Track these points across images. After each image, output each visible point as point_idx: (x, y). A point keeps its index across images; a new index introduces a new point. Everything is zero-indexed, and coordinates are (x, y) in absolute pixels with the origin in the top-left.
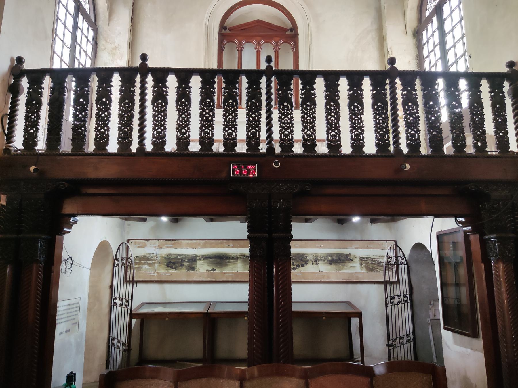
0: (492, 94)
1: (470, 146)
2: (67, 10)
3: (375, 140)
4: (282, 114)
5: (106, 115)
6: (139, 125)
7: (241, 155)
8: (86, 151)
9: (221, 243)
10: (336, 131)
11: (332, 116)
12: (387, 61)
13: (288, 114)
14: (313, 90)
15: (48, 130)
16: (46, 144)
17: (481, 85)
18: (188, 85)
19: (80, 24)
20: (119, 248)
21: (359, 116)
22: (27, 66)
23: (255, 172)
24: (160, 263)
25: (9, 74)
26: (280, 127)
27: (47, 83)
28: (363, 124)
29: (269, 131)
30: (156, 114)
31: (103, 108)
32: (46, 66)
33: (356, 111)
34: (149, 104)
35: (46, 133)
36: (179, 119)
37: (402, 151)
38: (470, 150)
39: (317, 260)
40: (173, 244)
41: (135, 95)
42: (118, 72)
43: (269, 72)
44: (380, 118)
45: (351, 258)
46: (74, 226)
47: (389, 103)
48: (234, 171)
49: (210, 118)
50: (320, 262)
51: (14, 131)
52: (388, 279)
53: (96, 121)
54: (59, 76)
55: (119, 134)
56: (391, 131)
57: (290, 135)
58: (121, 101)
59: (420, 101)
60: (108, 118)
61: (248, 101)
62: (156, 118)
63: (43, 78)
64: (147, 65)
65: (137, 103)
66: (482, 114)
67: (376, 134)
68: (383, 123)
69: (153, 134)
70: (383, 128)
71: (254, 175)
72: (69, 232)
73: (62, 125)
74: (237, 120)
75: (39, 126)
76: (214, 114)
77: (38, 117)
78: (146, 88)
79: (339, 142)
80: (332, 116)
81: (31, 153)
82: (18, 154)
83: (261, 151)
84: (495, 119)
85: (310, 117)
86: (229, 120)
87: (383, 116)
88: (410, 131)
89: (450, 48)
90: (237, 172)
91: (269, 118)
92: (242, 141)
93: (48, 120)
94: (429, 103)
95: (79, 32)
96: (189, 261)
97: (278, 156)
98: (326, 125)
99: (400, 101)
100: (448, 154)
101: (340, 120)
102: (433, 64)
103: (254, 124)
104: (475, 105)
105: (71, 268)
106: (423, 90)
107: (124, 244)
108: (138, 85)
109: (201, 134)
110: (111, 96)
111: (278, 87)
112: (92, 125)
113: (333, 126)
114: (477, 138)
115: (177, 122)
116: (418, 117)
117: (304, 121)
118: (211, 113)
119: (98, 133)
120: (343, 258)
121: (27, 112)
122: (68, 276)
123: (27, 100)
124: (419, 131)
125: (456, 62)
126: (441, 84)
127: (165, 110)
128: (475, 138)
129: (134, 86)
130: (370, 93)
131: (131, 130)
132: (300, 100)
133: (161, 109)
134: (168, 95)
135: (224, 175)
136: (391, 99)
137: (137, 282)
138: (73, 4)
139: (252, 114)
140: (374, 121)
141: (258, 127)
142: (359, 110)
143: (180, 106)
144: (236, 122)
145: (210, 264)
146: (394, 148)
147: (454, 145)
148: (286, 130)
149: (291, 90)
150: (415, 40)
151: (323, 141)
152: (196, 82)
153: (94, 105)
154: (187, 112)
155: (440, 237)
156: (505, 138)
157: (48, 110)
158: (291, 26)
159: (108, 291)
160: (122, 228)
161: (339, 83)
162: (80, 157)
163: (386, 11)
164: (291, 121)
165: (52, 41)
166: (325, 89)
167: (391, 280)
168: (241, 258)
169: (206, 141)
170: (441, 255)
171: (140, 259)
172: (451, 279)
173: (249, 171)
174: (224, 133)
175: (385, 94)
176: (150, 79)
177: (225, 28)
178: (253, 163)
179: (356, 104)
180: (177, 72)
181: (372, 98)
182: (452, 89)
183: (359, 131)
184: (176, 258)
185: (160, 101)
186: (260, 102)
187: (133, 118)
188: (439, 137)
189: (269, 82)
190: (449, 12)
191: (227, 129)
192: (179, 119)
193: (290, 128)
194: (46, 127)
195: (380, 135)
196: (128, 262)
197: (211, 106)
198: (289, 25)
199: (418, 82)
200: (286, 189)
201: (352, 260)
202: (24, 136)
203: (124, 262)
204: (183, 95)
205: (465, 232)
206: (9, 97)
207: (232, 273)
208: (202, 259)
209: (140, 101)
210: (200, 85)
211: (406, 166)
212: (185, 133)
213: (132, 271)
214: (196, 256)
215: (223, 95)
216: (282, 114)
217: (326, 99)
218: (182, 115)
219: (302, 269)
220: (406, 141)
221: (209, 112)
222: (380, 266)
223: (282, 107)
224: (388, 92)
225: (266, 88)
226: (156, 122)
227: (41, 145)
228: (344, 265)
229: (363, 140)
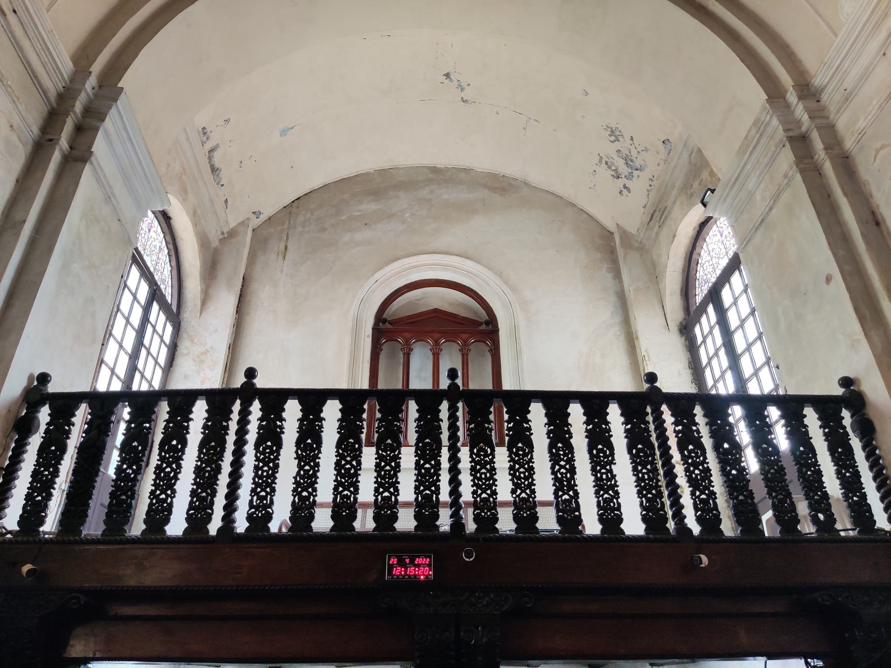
4: (477, 463)
7: (405, 536)
10: (571, 493)
11: (562, 467)
12: (643, 378)
13: (486, 463)
15: (69, 496)
17: (805, 416)
18: (319, 416)
21: (608, 467)
23: (430, 570)
25: (20, 402)
26: (472, 486)
27: (82, 415)
28: (616, 481)
31: (170, 457)
32: (85, 388)
33: (602, 458)
34: (250, 449)
37: (690, 531)
41: (227, 434)
43: (453, 394)
44: (644, 471)
47: (656, 445)
48: (391, 567)
53: (155, 480)
54: (103, 405)
55: (191, 502)
56: (666, 493)
59: (707, 442)
60: (176, 474)
62: (260, 472)
64: (254, 385)
65: (230, 447)
66: (816, 464)
67: (641, 498)
68: (650, 479)
69: (251, 502)
71: (427, 576)
73: (93, 487)
74: (399, 474)
77: (56, 473)
79: (577, 513)
80: (562, 467)
83: (442, 529)
84: (838, 472)
85: (524, 468)
89: (737, 329)
92: (407, 505)
97: (473, 538)
98: (552, 482)
99: (673, 442)
108: (235, 417)
111: (467, 418)
112: (147, 483)
115: (295, 478)
116: (708, 470)
118: (354, 463)
119: (154, 501)
123: (42, 443)
128: (810, 506)
130: (622, 428)
131: (214, 493)
133: (266, 481)
134: (283, 433)
136: (657, 438)
138: (147, 288)
140: (634, 475)
142: (606, 456)
143: (302, 452)
144: (397, 478)
146: (676, 524)
148: (484, 491)
149: (489, 422)
150: (683, 338)
152: (332, 411)
154: (314, 461)
161: (569, 411)
162: (116, 547)
163: (632, 296)
164: (492, 475)
166: (545, 420)
175: (647, 430)
176: (256, 408)
177: (384, 321)
179: (600, 447)
180: (302, 395)
181: (626, 437)
183: (610, 492)
185: (269, 443)
187: (220, 473)
189: (453, 410)
191: (381, 490)
193: (491, 488)
195: (648, 500)
198: (484, 316)
199: (698, 410)
204: (310, 433)
210: (339, 415)
211: (700, 558)
215: (377, 432)
216: (477, 463)
217: (549, 437)
218: (304, 466)
221: (352, 460)
223: (475, 451)
224: (652, 427)
225: (449, 419)
227: (50, 525)
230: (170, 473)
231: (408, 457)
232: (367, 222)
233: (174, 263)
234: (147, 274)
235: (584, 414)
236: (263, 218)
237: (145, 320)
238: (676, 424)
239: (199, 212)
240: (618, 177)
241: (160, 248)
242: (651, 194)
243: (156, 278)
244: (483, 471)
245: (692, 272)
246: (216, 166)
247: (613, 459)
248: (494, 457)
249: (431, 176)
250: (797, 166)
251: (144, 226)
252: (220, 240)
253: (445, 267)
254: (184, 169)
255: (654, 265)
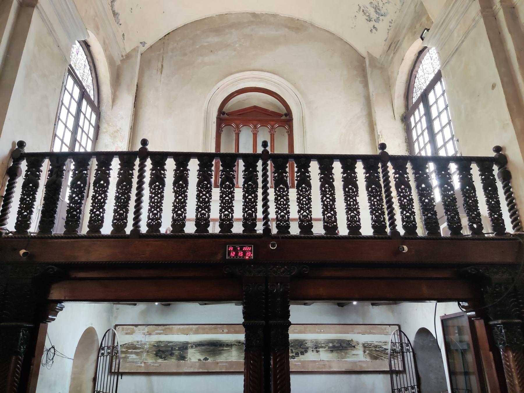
0: (483, 177)
1: (465, 226)
2: (72, 97)
3: (371, 222)
4: (278, 196)
5: (102, 198)
6: (135, 207)
7: (237, 236)
8: (79, 233)
9: (215, 328)
10: (332, 212)
11: (327, 198)
12: (378, 146)
13: (284, 196)
14: (308, 173)
15: (43, 212)
16: (39, 226)
17: (471, 169)
19: (83, 109)
20: (105, 335)
21: (354, 198)
22: (27, 150)
24: (148, 352)
26: (276, 208)
27: (46, 166)
28: (358, 206)
29: (266, 212)
30: (153, 195)
31: (100, 191)
32: (46, 150)
34: (146, 187)
35: (40, 215)
36: (175, 200)
37: (399, 233)
38: (466, 232)
39: (317, 347)
40: (163, 330)
41: (133, 178)
42: (118, 156)
43: (265, 156)
44: (375, 200)
45: (353, 345)
46: (60, 313)
47: (383, 185)
48: (229, 252)
49: (207, 199)
50: (320, 349)
51: (7, 213)
52: (393, 369)
54: (58, 160)
55: (114, 216)
57: (286, 216)
58: (119, 184)
59: (413, 184)
60: (105, 200)
61: (245, 183)
62: (153, 200)
63: (42, 161)
64: (146, 149)
65: (135, 185)
66: (475, 196)
68: (378, 205)
69: (149, 216)
70: (379, 209)
72: (54, 320)
73: (57, 207)
74: (233, 202)
75: (33, 208)
76: (210, 195)
77: (34, 200)
78: (145, 171)
79: (335, 224)
80: (327, 198)
81: (23, 236)
82: (8, 237)
83: (258, 232)
84: (488, 201)
86: (226, 201)
87: (378, 198)
88: (405, 212)
90: (233, 254)
91: (265, 200)
92: (238, 220)
93: (43, 202)
94: (421, 186)
95: (82, 117)
96: (179, 349)
97: (275, 237)
98: (322, 206)
99: (392, 184)
100: (445, 236)
101: (335, 201)
102: (423, 148)
103: (250, 205)
104: (467, 188)
105: (52, 359)
106: (415, 173)
107: (111, 331)
108: (137, 167)
109: (197, 216)
110: (110, 179)
111: (273, 169)
112: (88, 206)
113: (329, 207)
114: (472, 220)
115: (173, 203)
116: (412, 199)
117: (299, 203)
118: (208, 195)
119: (93, 215)
120: (345, 345)
121: (23, 194)
122: (49, 368)
124: (414, 212)
125: (445, 145)
126: (431, 167)
127: (162, 192)
128: (470, 220)
129: (133, 169)
131: (127, 211)
132: (296, 182)
134: (165, 177)
135: (219, 257)
136: (384, 182)
137: (122, 374)
139: (248, 196)
140: (369, 202)
141: (254, 208)
142: (353, 192)
143: (177, 188)
144: (232, 204)
145: (202, 352)
146: (391, 229)
147: (450, 227)
148: (282, 211)
149: (286, 173)
150: (403, 124)
151: (319, 220)
152: (193, 165)
153: (92, 187)
154: (184, 193)
155: (445, 322)
156: (500, 220)
157: (44, 192)
158: (286, 112)
159: (91, 384)
160: (110, 312)
163: (374, 99)
165: (55, 125)
166: (319, 171)
167: (397, 369)
168: (234, 344)
169: (202, 222)
170: (447, 340)
171: (127, 348)
172: (459, 367)
173: (245, 253)
174: (221, 214)
175: (378, 177)
177: (224, 113)
178: (248, 244)
179: (350, 186)
181: (366, 181)
182: (443, 172)
183: (355, 212)
184: (166, 346)
185: (157, 184)
186: (257, 184)
187: (130, 200)
188: (434, 219)
189: (265, 165)
190: (434, 100)
192: (175, 201)
194: (41, 208)
195: (376, 216)
196: (113, 352)
197: (208, 188)
198: (284, 110)
199: (409, 166)
200: (284, 272)
201: (354, 347)
202: (18, 218)
203: (109, 351)
204: (181, 178)
205: (470, 318)
206: (6, 180)
207: (227, 362)
208: (194, 346)
209: (138, 183)
210: (198, 168)
212: (181, 215)
213: (118, 361)
214: (187, 343)
215: (221, 178)
216: (278, 196)
217: (320, 181)
218: (178, 196)
219: (302, 358)
220: (401, 223)
221: (206, 194)
222: (384, 353)
224: (381, 175)
225: (262, 171)
226: (153, 203)
227: (34, 228)
228: (346, 353)
229: (359, 221)
230: (101, 199)
231: (239, 194)
232: (212, 49)
233: (94, 75)
234: (78, 82)
235: (342, 168)
236: (147, 46)
237: (79, 110)
238: (395, 173)
239: (107, 41)
240: (370, 21)
241: (85, 65)
242: (390, 32)
243: (84, 84)
244: (282, 200)
245: (412, 83)
246: (116, 11)
247: (358, 193)
248: (288, 192)
249: (252, 19)
250: (482, 13)
251: (74, 50)
252: (121, 61)
253: (261, 79)
254: (96, 13)
255: (389, 79)
